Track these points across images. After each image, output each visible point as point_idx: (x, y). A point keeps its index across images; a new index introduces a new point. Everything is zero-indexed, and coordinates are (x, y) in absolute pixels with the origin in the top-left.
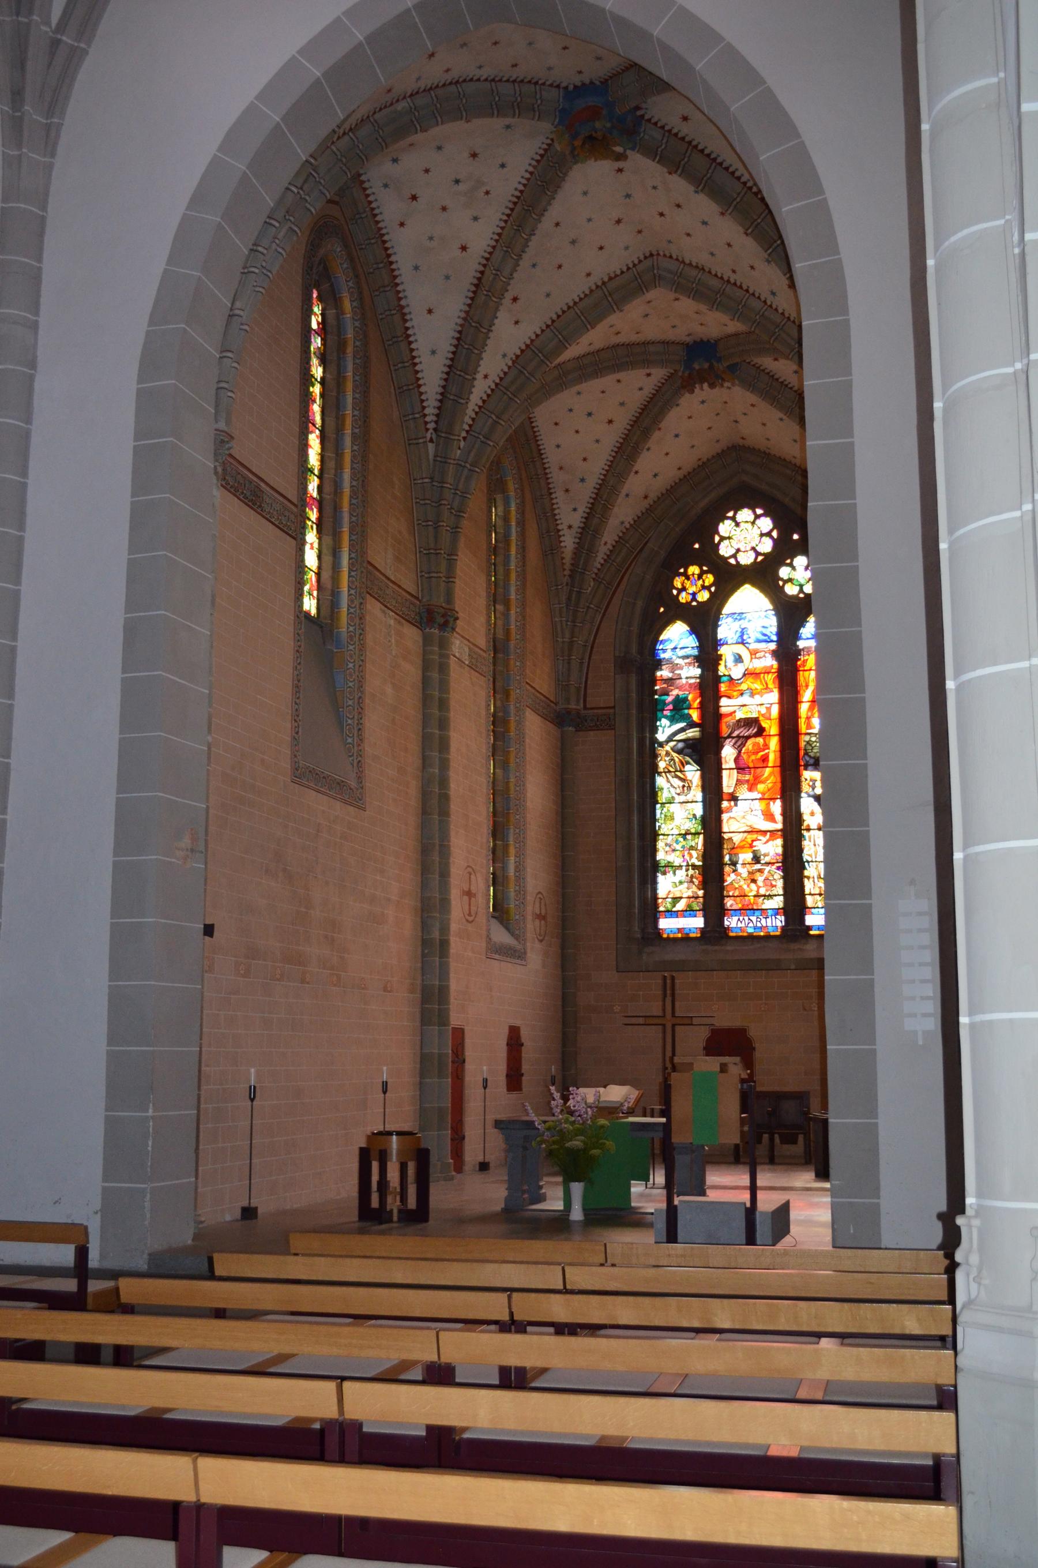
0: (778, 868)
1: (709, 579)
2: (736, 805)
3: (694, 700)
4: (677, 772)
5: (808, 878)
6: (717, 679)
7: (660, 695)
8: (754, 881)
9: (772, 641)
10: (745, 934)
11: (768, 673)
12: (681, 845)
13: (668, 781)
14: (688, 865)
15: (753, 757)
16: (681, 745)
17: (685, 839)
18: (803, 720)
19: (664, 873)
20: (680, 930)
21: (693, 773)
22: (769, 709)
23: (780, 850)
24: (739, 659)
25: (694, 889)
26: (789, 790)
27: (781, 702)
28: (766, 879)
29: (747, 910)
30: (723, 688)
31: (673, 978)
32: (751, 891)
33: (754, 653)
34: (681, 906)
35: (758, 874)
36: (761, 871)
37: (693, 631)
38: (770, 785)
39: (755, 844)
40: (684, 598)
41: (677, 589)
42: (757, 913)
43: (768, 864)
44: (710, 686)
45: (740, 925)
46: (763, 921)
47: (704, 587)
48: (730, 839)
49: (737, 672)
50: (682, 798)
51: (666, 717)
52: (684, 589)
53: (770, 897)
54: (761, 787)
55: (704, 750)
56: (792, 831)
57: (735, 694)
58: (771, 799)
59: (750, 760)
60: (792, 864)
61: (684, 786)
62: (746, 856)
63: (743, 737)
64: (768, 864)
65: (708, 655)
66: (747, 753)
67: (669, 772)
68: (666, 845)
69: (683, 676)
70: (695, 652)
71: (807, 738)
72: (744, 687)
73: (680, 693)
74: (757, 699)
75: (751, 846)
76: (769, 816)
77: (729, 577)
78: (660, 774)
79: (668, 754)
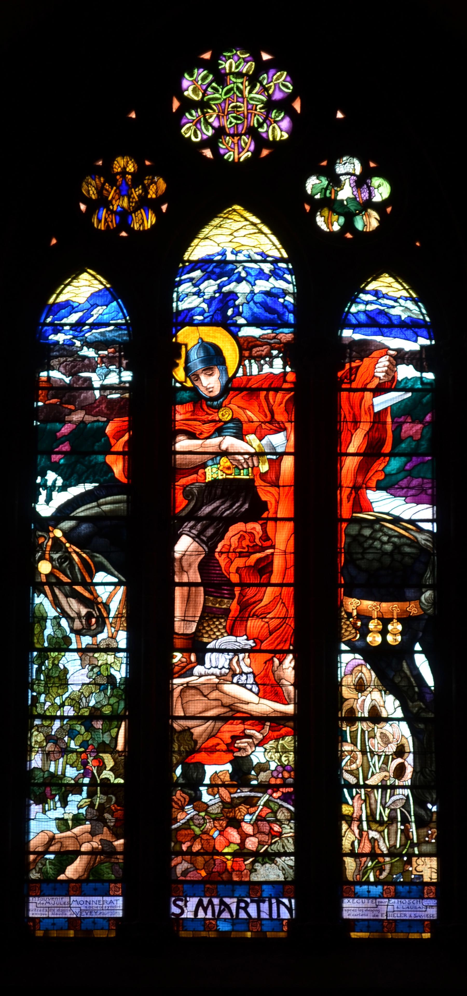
0: (285, 797)
1: (158, 187)
2: (201, 661)
3: (118, 435)
4: (74, 583)
5: (350, 819)
6: (169, 395)
7: (44, 422)
8: (236, 823)
9: (287, 325)
10: (212, 935)
11: (277, 390)
12: (80, 739)
13: (56, 603)
14: (93, 784)
15: (239, 562)
16: (84, 528)
17: (89, 728)
18: (346, 492)
19: (42, 800)
20: (73, 922)
21: (109, 590)
22: (275, 464)
23: (289, 759)
24: (213, 357)
25: (106, 834)
26: (314, 641)
27: (299, 453)
28: (260, 818)
29: (218, 883)
30: (181, 414)
31: (194, 621)
32: (229, 843)
33: (246, 348)
34: (72, 871)
35: (243, 808)
36: (250, 802)
37: (116, 291)
38: (274, 623)
39: (240, 743)
40: (102, 221)
41: (87, 200)
42: (240, 891)
43: (263, 787)
44: (153, 406)
45: (201, 914)
46: (252, 910)
47: (145, 203)
48: (188, 730)
49: (211, 383)
50: (86, 641)
51: (56, 468)
52: (103, 202)
53: (269, 857)
54: (254, 625)
55: (135, 539)
56: (319, 721)
57: (206, 428)
58: (274, 652)
59: (232, 568)
60: (316, 787)
61: (89, 616)
62: (216, 769)
63: (220, 518)
64: (263, 787)
65: (149, 339)
66: (226, 552)
67: (60, 584)
68: (48, 738)
69: (97, 384)
70: (123, 335)
71: (354, 529)
72: (225, 415)
73: (89, 418)
74: (253, 443)
75: (230, 748)
76: (269, 688)
77: (204, 189)
78: (39, 589)
79: (57, 545)
